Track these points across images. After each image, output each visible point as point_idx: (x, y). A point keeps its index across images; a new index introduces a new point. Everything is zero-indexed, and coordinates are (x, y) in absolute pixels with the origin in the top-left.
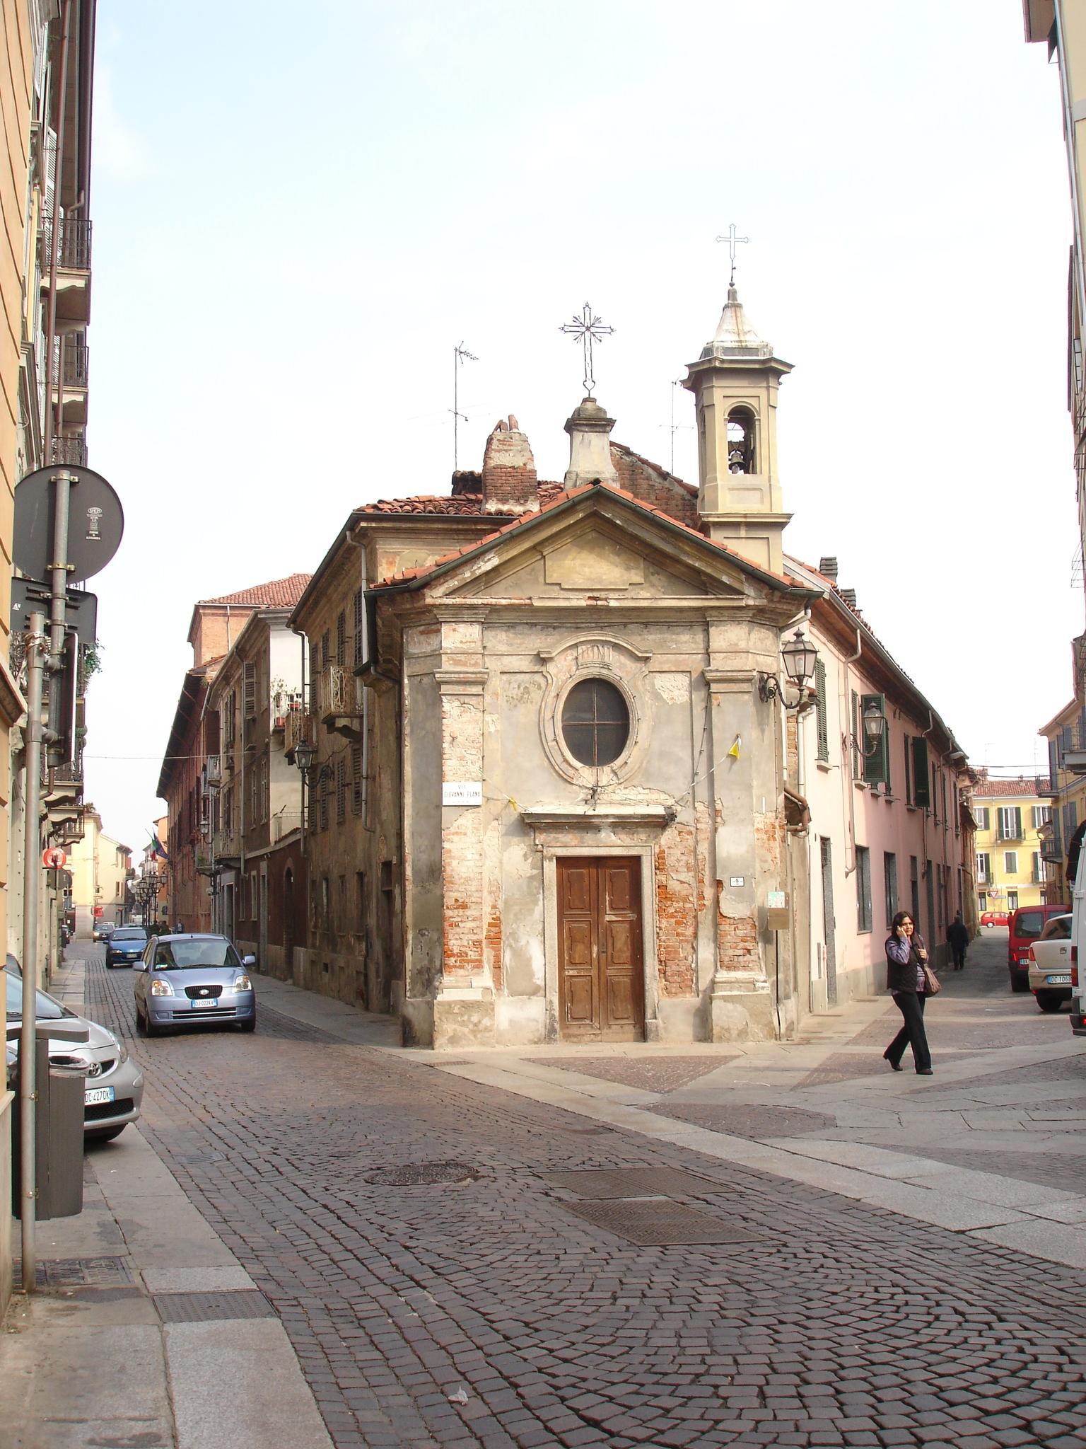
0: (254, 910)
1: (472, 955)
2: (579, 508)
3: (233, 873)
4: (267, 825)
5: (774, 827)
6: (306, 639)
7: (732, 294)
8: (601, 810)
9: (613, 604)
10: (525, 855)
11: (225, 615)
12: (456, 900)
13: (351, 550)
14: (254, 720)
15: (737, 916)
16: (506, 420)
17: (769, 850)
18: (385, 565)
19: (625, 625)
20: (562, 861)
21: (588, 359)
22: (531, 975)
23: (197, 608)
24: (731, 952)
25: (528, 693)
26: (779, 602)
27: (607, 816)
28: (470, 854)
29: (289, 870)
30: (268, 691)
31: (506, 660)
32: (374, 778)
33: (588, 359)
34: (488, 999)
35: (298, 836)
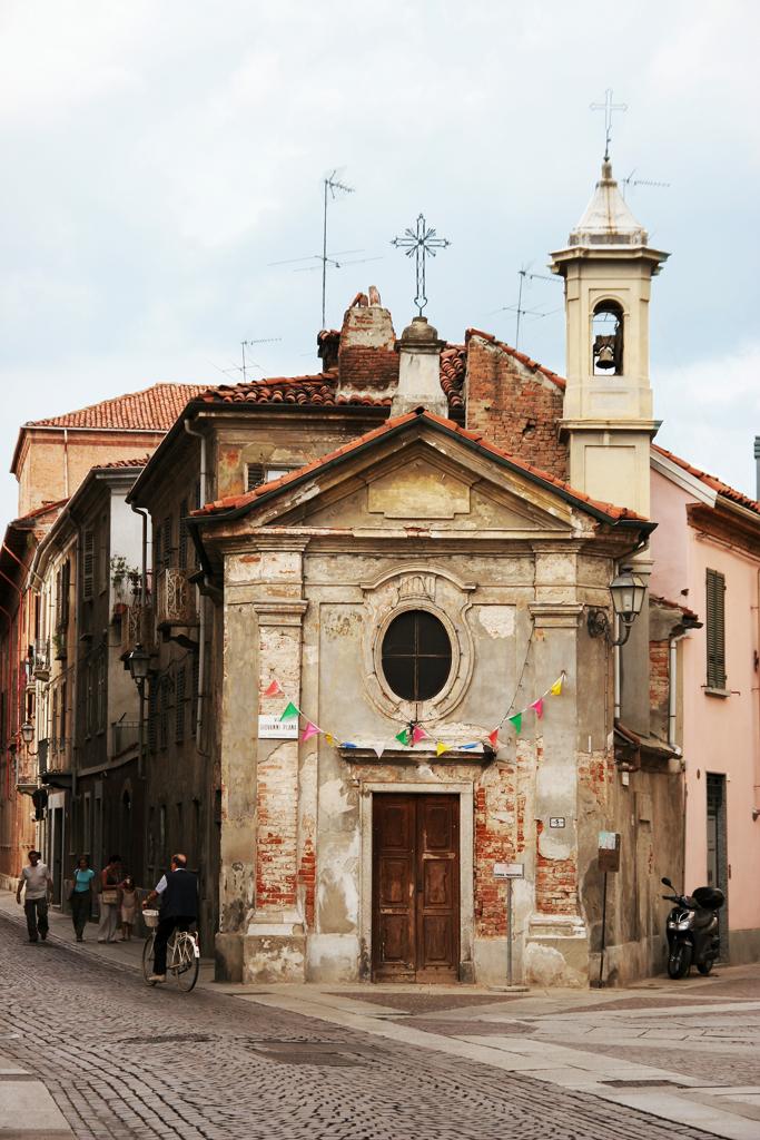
0: (86, 844)
1: (284, 890)
2: (402, 437)
3: (63, 793)
4: (103, 736)
5: (602, 767)
6: (149, 517)
7: (607, 171)
8: (419, 747)
9: (435, 535)
10: (341, 790)
11: (62, 442)
12: (270, 835)
13: (192, 443)
14: (91, 602)
15: (557, 858)
16: (366, 293)
17: (595, 791)
18: (225, 460)
19: (450, 556)
20: (377, 796)
21: (421, 274)
22: (344, 912)
23: (23, 432)
24: (549, 895)
25: (349, 624)
26: (609, 534)
27: (424, 752)
28: (287, 788)
29: (126, 793)
30: (108, 573)
31: (326, 591)
32: (211, 698)
33: (421, 274)
34: (300, 935)
35: (136, 754)
